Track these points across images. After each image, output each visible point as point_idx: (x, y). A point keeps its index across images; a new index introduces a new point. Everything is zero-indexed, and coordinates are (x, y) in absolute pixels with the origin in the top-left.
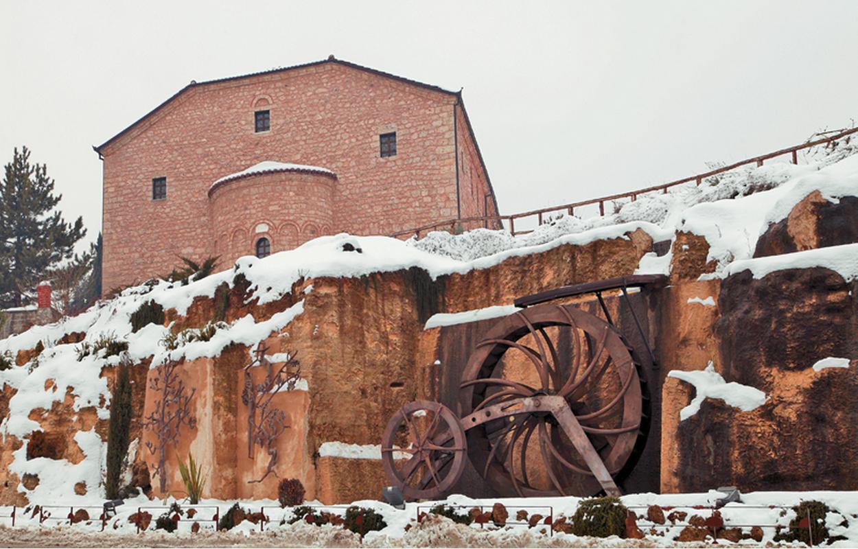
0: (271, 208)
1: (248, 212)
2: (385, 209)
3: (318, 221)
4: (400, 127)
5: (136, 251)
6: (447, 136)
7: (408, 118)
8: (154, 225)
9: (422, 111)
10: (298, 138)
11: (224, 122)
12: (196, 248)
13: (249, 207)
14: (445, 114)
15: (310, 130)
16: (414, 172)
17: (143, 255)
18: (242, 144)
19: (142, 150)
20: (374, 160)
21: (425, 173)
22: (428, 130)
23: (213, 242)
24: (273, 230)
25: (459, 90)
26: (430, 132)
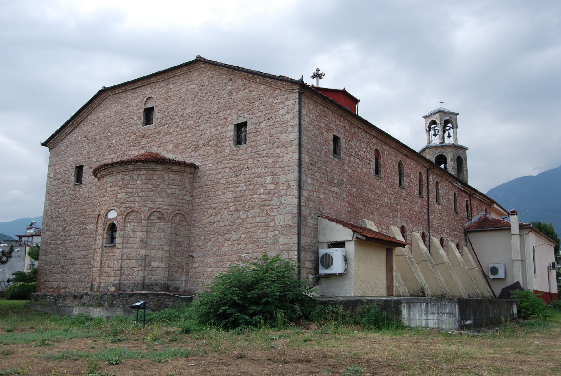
0: (119, 196)
2: (235, 195)
3: (166, 207)
4: (251, 116)
6: (291, 124)
9: (271, 100)
10: (171, 130)
14: (290, 103)
15: (182, 122)
16: (261, 159)
17: (64, 229)
18: (133, 137)
21: (270, 160)
25: (300, 78)
26: (276, 120)
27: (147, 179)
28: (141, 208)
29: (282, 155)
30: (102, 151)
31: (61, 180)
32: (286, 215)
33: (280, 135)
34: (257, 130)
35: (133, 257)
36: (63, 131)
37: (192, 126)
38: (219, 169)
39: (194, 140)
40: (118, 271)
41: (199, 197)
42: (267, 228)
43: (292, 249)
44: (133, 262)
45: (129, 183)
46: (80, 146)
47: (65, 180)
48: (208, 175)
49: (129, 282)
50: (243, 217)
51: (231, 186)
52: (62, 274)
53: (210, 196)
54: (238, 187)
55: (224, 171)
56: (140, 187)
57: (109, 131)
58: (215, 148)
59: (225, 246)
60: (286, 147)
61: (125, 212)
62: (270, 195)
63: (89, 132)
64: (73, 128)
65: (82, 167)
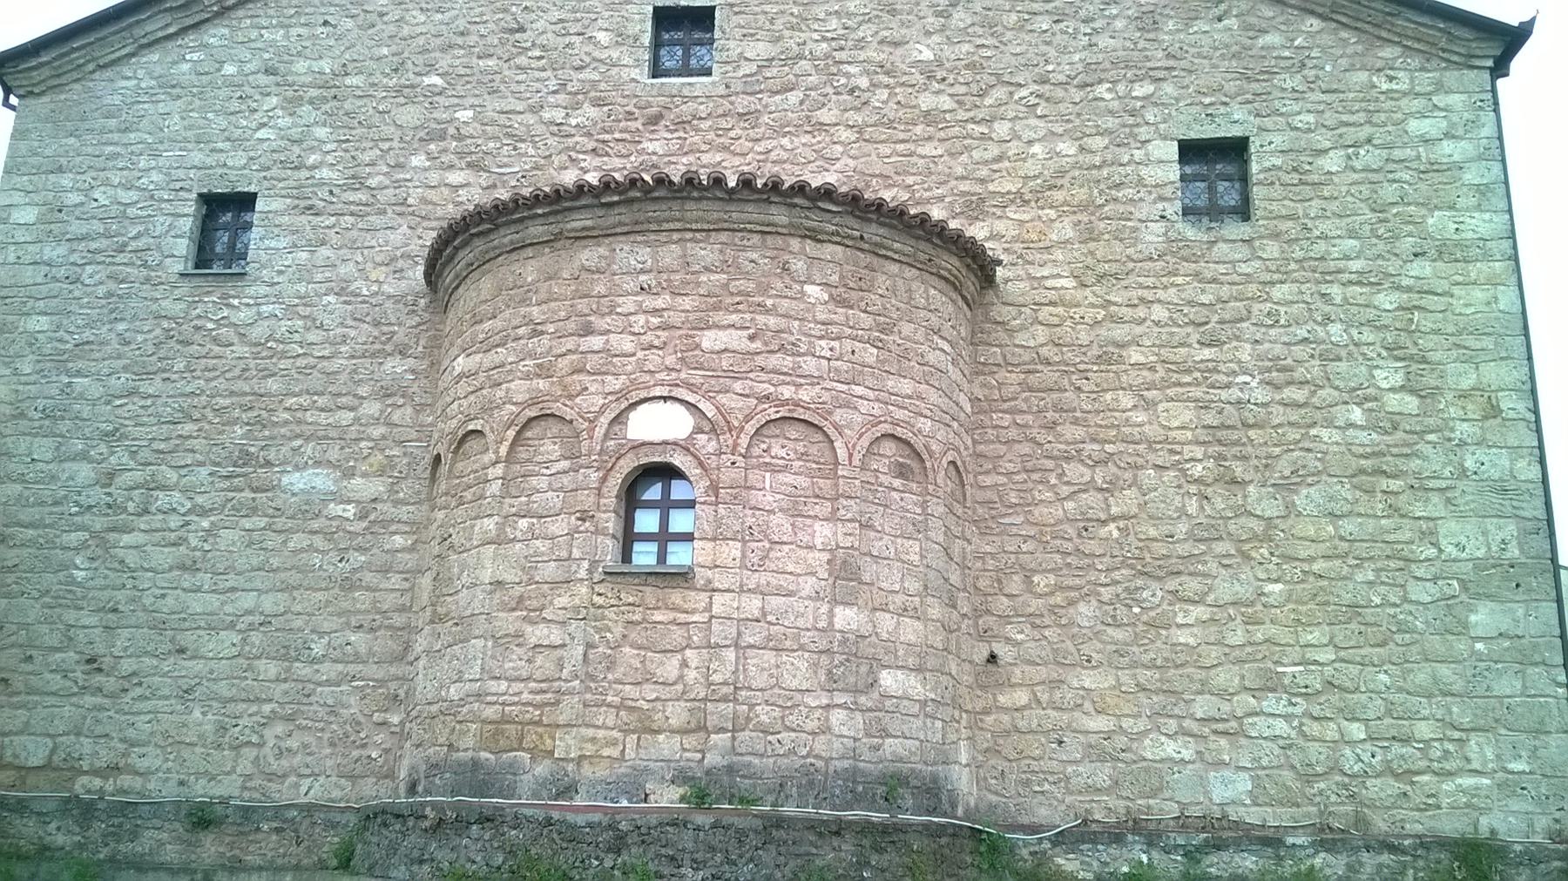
0: (710, 340)
1: (596, 342)
2: (1210, 418)
4: (1268, 122)
5: (83, 456)
7: (1298, 95)
8: (180, 365)
10: (825, 116)
11: (522, 29)
12: (349, 474)
13: (600, 323)
17: (111, 475)
18: (593, 112)
19: (170, 87)
20: (1159, 227)
22: (1389, 147)
23: (428, 458)
24: (714, 431)
26: (1398, 154)
27: (851, 285)
28: (830, 413)
29: (1443, 285)
30: (386, 146)
31: (94, 245)
32: (1495, 520)
33: (1424, 211)
34: (1303, 180)
35: (797, 637)
36: (130, 26)
37: (948, 116)
38: (1115, 304)
39: (959, 171)
40: (722, 706)
41: (1006, 406)
42: (1401, 564)
43: (1537, 658)
44: (801, 662)
45: (764, 289)
46: (235, 105)
47: (125, 245)
48: (1056, 320)
49: (780, 761)
50: (1271, 508)
51: (1187, 379)
52: (89, 700)
53: (1074, 410)
54: (1228, 386)
55: (1141, 312)
56: (821, 317)
57: (430, 68)
58: (1084, 218)
59: (1179, 626)
60: (1457, 261)
61: (748, 418)
62: (1400, 435)
63: (299, 54)
64: (189, 22)
65: (245, 202)
